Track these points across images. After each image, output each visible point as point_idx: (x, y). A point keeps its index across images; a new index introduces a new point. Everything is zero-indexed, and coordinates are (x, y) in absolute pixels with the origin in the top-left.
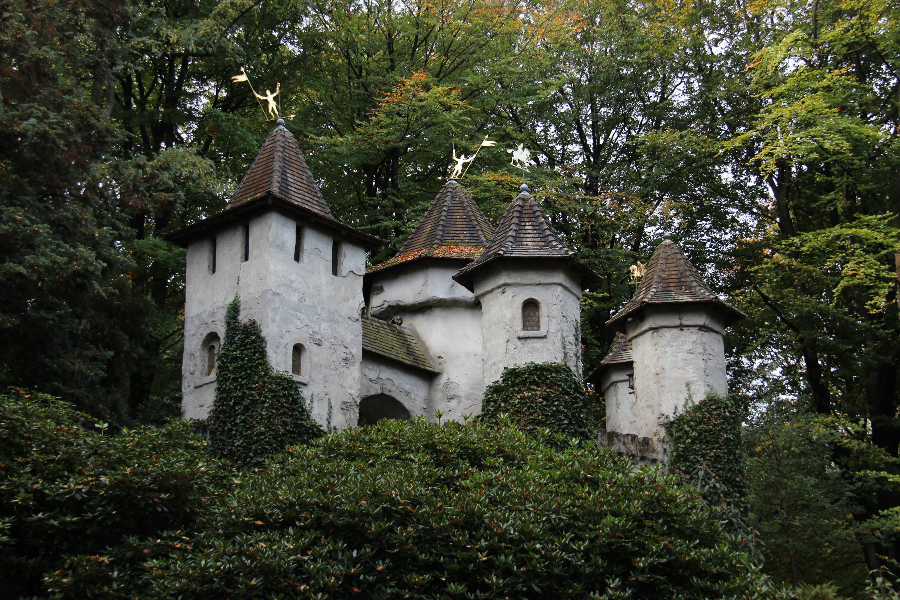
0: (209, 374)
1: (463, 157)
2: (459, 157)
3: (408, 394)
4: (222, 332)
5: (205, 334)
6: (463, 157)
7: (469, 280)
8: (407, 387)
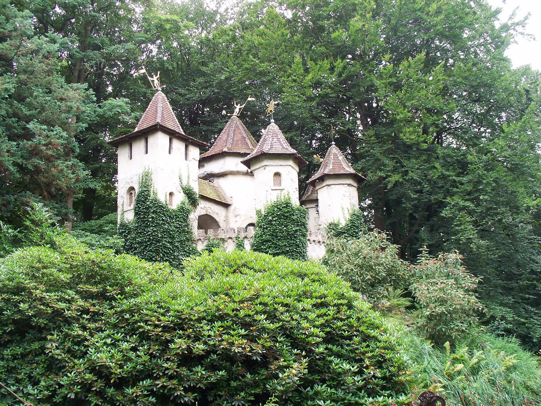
0: (130, 205)
1: (239, 105)
2: (237, 105)
3: (217, 214)
4: (137, 187)
5: (128, 188)
6: (239, 105)
7: (248, 163)
8: (217, 211)
